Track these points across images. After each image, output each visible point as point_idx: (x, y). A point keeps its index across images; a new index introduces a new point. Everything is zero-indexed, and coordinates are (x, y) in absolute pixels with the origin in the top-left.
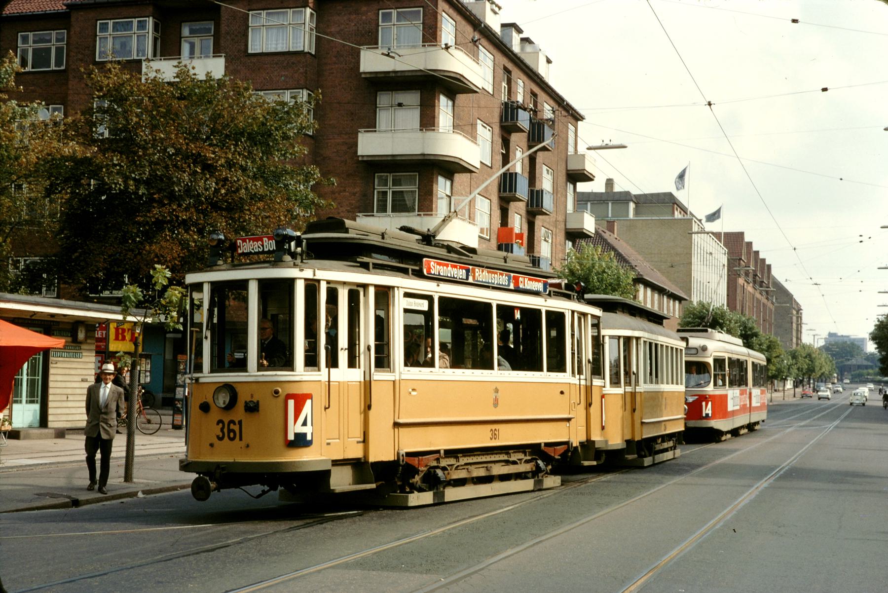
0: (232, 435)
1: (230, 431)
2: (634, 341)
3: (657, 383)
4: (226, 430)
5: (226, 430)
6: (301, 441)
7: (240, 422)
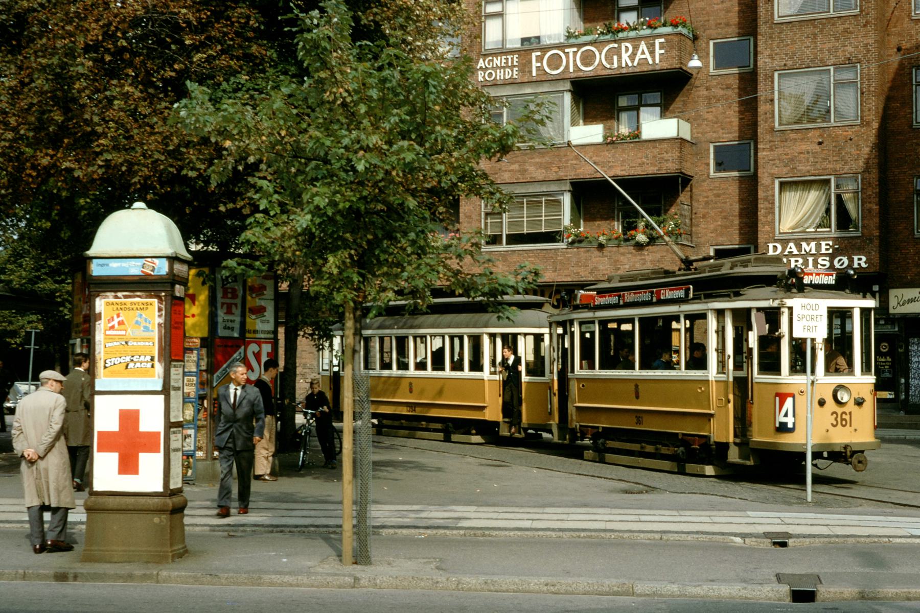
0: (844, 423)
1: (842, 419)
2: (377, 340)
3: (341, 503)
4: (839, 419)
5: (839, 419)
6: (783, 428)
7: (850, 413)
